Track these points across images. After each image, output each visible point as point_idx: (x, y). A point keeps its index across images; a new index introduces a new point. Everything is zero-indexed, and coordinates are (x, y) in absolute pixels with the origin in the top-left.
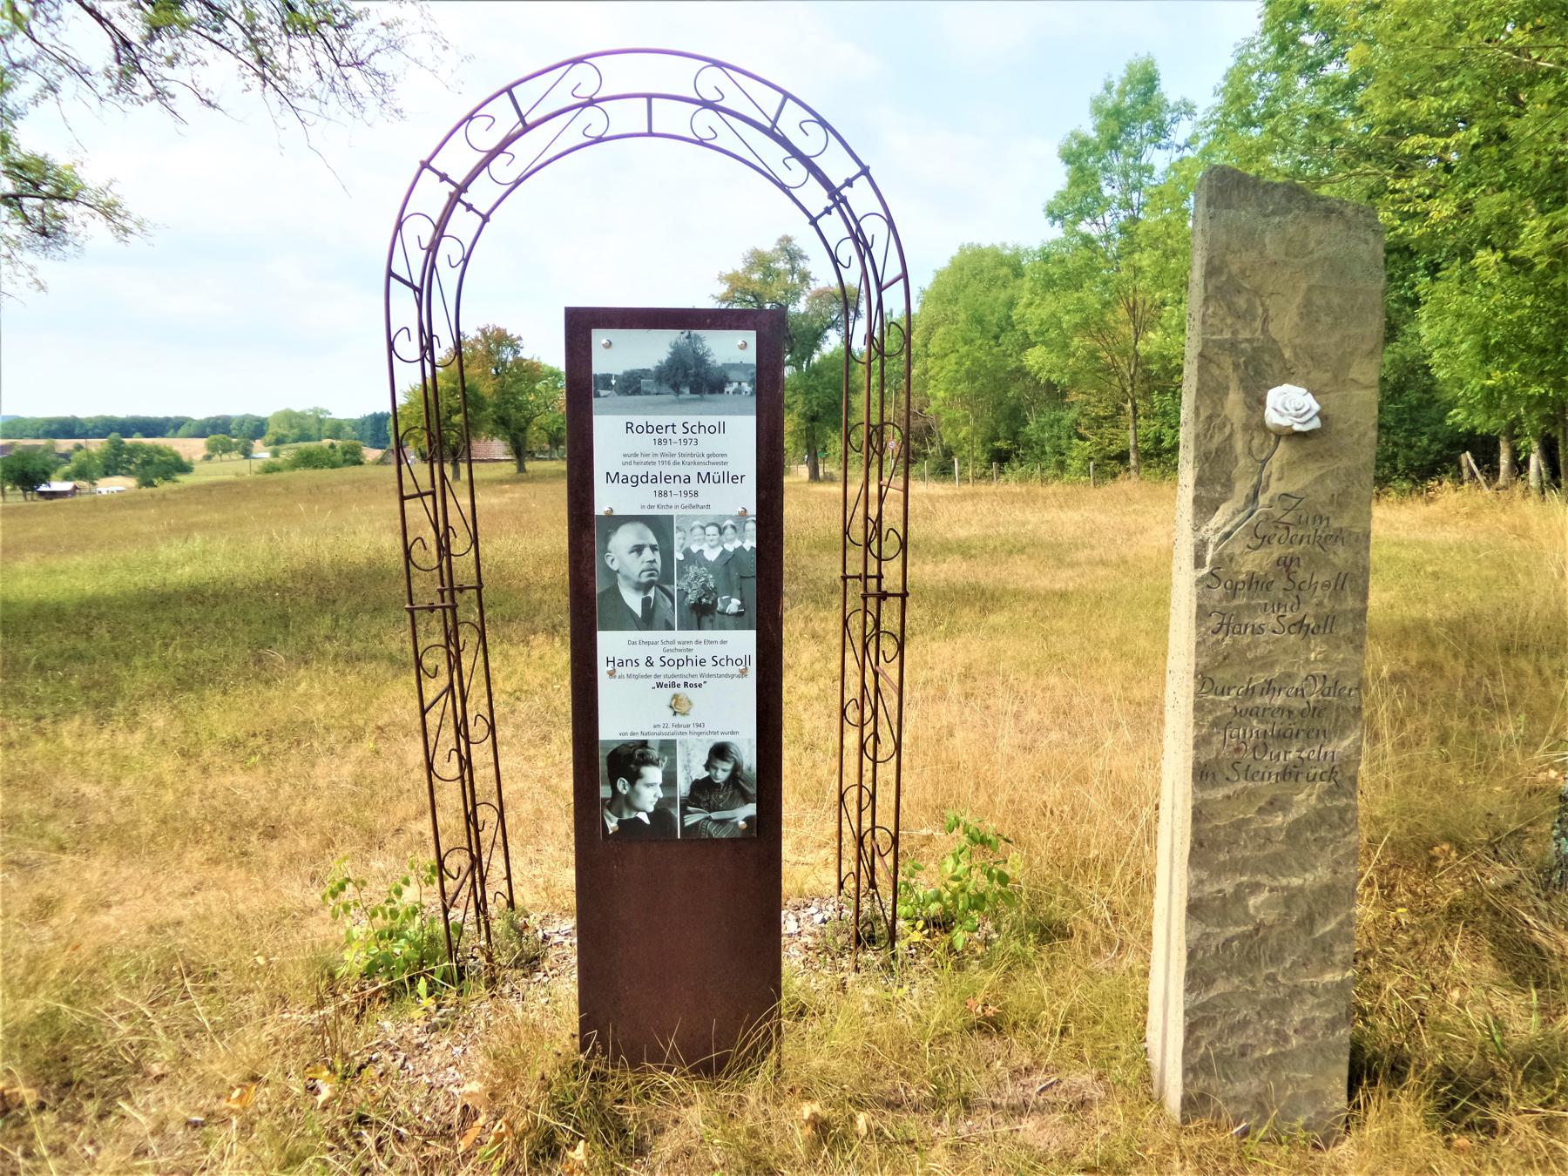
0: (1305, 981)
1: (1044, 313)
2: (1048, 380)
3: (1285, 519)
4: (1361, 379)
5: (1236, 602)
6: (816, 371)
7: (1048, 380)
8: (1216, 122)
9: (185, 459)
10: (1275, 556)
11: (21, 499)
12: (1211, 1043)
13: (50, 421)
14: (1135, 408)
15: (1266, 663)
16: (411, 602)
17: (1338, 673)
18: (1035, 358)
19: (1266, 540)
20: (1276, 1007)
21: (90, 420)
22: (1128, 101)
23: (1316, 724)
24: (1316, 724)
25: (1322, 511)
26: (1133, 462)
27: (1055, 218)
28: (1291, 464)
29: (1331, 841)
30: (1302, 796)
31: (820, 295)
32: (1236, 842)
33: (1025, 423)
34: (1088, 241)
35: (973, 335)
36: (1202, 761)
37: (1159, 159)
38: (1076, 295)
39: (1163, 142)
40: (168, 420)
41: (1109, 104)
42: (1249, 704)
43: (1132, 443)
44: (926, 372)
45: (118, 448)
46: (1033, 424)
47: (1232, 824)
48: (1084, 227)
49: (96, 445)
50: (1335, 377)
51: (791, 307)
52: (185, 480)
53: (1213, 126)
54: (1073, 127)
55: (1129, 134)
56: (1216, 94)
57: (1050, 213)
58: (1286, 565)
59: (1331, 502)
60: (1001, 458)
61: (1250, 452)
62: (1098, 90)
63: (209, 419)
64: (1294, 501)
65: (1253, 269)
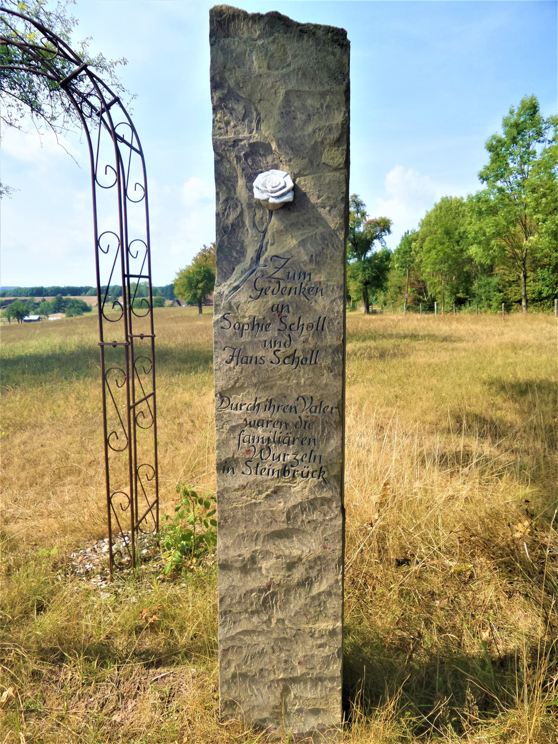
0: (306, 627)
1: (476, 228)
3: (276, 275)
4: (331, 162)
5: (243, 339)
6: (370, 260)
9: (88, 305)
10: (270, 304)
11: (17, 323)
12: (239, 665)
13: (32, 289)
14: (525, 277)
17: (322, 395)
18: (474, 250)
19: (263, 292)
20: (284, 642)
21: (49, 288)
22: (522, 119)
23: (307, 434)
24: (307, 434)
25: (305, 269)
26: (524, 303)
27: (484, 180)
28: (280, 233)
29: (321, 523)
30: (298, 488)
31: (370, 223)
32: (251, 520)
33: (472, 284)
34: (501, 190)
35: (444, 241)
36: (223, 459)
37: (538, 147)
38: (493, 218)
39: (541, 139)
40: (82, 288)
41: (512, 121)
43: (523, 294)
44: (421, 261)
45: (60, 301)
46: (476, 285)
47: (246, 507)
48: (499, 184)
49: (50, 299)
50: (311, 162)
51: (356, 229)
52: (86, 314)
54: (493, 133)
55: (523, 136)
58: (278, 311)
59: (311, 261)
60: (460, 303)
61: (254, 225)
62: (507, 114)
64: (282, 262)
65: (244, 82)
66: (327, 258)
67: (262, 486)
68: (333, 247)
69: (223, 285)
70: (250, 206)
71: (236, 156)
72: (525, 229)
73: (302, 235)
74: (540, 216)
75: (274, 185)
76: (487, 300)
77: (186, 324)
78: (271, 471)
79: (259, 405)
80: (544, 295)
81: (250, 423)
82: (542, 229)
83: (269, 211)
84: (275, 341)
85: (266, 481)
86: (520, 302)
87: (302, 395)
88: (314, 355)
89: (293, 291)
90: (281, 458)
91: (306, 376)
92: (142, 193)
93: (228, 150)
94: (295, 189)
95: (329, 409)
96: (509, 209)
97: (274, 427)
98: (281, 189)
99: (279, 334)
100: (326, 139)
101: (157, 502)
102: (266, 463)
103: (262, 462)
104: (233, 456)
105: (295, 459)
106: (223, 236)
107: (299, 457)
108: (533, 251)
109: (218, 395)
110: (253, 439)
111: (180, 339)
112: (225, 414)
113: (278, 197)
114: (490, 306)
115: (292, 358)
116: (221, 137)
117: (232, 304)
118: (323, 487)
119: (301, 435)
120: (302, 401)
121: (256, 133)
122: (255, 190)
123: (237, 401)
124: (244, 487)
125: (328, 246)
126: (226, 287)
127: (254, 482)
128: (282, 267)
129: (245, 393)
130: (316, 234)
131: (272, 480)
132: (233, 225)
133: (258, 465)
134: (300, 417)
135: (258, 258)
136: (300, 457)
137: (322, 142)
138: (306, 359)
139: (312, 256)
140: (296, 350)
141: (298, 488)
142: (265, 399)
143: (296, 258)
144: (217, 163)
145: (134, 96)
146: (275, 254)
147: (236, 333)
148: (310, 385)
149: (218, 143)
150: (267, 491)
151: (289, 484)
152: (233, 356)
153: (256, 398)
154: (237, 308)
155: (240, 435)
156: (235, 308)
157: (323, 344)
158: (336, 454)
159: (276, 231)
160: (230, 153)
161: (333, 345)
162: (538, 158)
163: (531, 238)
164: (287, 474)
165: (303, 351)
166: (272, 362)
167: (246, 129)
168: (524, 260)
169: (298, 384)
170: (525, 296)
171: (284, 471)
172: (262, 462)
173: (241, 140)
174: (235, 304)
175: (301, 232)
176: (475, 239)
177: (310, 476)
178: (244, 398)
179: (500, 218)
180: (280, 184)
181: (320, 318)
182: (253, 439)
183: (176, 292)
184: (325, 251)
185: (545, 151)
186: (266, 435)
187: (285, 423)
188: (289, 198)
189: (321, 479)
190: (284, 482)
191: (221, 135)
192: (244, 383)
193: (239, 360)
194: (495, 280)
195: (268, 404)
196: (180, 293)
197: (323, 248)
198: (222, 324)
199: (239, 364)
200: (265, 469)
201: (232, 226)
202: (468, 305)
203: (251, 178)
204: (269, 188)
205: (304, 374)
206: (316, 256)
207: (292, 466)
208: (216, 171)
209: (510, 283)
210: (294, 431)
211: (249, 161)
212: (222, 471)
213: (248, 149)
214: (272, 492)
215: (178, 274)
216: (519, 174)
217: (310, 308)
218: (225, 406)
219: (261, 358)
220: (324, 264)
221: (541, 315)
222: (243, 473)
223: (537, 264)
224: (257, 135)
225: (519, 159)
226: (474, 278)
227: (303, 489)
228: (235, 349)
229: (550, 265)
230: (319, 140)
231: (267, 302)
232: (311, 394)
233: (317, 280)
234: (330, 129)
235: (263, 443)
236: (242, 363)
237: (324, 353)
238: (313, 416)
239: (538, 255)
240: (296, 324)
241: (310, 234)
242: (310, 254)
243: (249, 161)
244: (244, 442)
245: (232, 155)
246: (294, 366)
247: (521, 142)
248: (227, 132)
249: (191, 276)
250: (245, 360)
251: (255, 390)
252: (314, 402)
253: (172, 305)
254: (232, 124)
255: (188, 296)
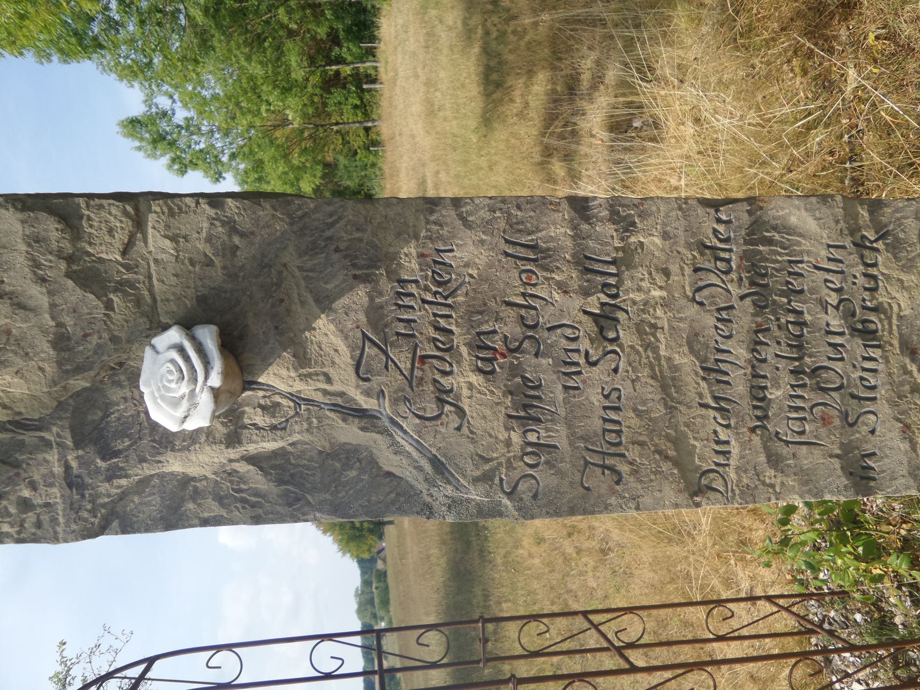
2: (321, 178)
3: (405, 365)
4: (121, 237)
5: (562, 443)
7: (321, 178)
8: (150, 86)
10: (475, 379)
14: (337, 124)
15: (668, 383)
16: (478, 662)
17: (689, 246)
22: (147, 135)
26: (370, 124)
28: (302, 359)
30: (902, 298)
33: (347, 188)
34: (233, 156)
37: (181, 115)
41: (149, 147)
42: (746, 404)
43: (358, 125)
46: (348, 183)
48: (225, 159)
53: (154, 87)
55: (167, 133)
56: (132, 86)
57: (217, 180)
59: (366, 279)
63: (364, 657)
64: (369, 350)
66: (360, 240)
67: (902, 384)
68: (332, 225)
69: (429, 499)
70: (233, 440)
71: (109, 479)
72: (279, 126)
73: (303, 303)
74: (264, 108)
75: (176, 375)
76: (366, 169)
77: (408, 541)
78: (868, 365)
79: (716, 399)
80: (358, 103)
81: (758, 418)
82: (279, 106)
83: (244, 389)
84: (566, 363)
85: (890, 374)
86: (367, 129)
87: (690, 294)
88: (597, 267)
89: (442, 322)
90: (838, 340)
91: (645, 284)
92: (224, 654)
93: (93, 501)
94: (187, 325)
95: (721, 228)
96: (255, 146)
97: (764, 361)
98: (187, 359)
99: (545, 355)
100: (60, 250)
101: (769, 598)
102: (849, 377)
103: (849, 386)
104: (837, 456)
105: (837, 308)
106: (309, 503)
107: (833, 299)
108: (305, 116)
109: (697, 499)
110: (797, 409)
111: (435, 551)
112: (740, 480)
113: (207, 364)
114: (374, 165)
115: (603, 322)
116: (61, 520)
117: (478, 473)
118: (897, 239)
119: (782, 294)
120: (706, 292)
121: (48, 429)
122: (191, 425)
123: (708, 453)
124: (907, 427)
125: (330, 238)
126: (434, 491)
127: (893, 404)
128: (385, 353)
129: (690, 435)
130: (300, 268)
131: (887, 361)
132: (280, 482)
133: (853, 396)
134: (742, 298)
135: (362, 414)
136: (833, 294)
137: (70, 259)
138: (606, 285)
139: (355, 277)
140: (585, 312)
141: (902, 298)
142: (703, 384)
143: (362, 318)
144: (127, 528)
145: (107, 630)
146: (351, 371)
147: (547, 462)
148: (666, 273)
149: (74, 527)
150: (910, 373)
151: (895, 321)
152: (604, 467)
153: (701, 405)
154: (488, 460)
155: (787, 443)
156: (487, 467)
157: (569, 243)
158: (824, 209)
159: (296, 369)
160: (98, 496)
161: (572, 220)
162: (192, 114)
163: (290, 118)
164: (872, 327)
165: (586, 293)
166: (616, 370)
167: (40, 456)
168: (316, 126)
169: (666, 304)
170: (360, 122)
171: (867, 334)
172: (849, 386)
173: (67, 467)
174: (477, 467)
175: (297, 307)
176: (292, 185)
177: (873, 271)
178: (702, 435)
179: (266, 155)
180: (173, 361)
181: (507, 255)
182: (797, 409)
183: (366, 556)
184: (342, 245)
185: (185, 106)
186: (786, 379)
187: (756, 332)
188: (208, 336)
189: (880, 245)
190: (891, 333)
191: (54, 521)
192: (668, 438)
193: (613, 450)
194: (342, 161)
195: (713, 376)
196: (369, 550)
197: (337, 250)
198: (527, 497)
199: (621, 450)
200: (862, 378)
201: (285, 483)
202: (373, 192)
203: (165, 441)
204: (184, 388)
205: (639, 289)
206: (354, 266)
207: (853, 314)
208: (148, 530)
209: (345, 143)
210: (774, 312)
211: (120, 445)
212: (872, 484)
213: (91, 449)
214: (913, 360)
215: (344, 554)
216: (213, 135)
217: (483, 278)
218: (721, 481)
219: (607, 397)
220: (375, 247)
221: (384, 103)
222: (873, 432)
223: (321, 111)
224: (55, 429)
225: (194, 137)
226: (340, 186)
227: (903, 288)
228: (587, 463)
229: (322, 95)
230: (63, 266)
231: (471, 386)
232: (688, 271)
233: (415, 265)
234: (36, 240)
235: (804, 386)
236: (619, 444)
237: (591, 243)
238: (739, 267)
239: (311, 111)
240: (523, 312)
241: (303, 282)
242: (351, 281)
243: (120, 445)
244: (802, 433)
245: (107, 490)
246: (621, 316)
247: (175, 136)
248: (47, 505)
249: (346, 537)
250: (612, 437)
251: (682, 408)
252: (707, 265)
253: (384, 560)
254: (26, 493)
255: (371, 539)
